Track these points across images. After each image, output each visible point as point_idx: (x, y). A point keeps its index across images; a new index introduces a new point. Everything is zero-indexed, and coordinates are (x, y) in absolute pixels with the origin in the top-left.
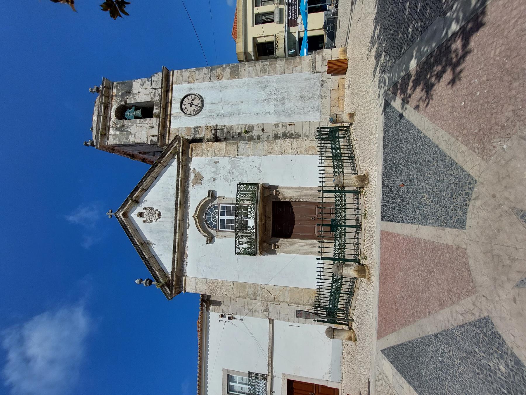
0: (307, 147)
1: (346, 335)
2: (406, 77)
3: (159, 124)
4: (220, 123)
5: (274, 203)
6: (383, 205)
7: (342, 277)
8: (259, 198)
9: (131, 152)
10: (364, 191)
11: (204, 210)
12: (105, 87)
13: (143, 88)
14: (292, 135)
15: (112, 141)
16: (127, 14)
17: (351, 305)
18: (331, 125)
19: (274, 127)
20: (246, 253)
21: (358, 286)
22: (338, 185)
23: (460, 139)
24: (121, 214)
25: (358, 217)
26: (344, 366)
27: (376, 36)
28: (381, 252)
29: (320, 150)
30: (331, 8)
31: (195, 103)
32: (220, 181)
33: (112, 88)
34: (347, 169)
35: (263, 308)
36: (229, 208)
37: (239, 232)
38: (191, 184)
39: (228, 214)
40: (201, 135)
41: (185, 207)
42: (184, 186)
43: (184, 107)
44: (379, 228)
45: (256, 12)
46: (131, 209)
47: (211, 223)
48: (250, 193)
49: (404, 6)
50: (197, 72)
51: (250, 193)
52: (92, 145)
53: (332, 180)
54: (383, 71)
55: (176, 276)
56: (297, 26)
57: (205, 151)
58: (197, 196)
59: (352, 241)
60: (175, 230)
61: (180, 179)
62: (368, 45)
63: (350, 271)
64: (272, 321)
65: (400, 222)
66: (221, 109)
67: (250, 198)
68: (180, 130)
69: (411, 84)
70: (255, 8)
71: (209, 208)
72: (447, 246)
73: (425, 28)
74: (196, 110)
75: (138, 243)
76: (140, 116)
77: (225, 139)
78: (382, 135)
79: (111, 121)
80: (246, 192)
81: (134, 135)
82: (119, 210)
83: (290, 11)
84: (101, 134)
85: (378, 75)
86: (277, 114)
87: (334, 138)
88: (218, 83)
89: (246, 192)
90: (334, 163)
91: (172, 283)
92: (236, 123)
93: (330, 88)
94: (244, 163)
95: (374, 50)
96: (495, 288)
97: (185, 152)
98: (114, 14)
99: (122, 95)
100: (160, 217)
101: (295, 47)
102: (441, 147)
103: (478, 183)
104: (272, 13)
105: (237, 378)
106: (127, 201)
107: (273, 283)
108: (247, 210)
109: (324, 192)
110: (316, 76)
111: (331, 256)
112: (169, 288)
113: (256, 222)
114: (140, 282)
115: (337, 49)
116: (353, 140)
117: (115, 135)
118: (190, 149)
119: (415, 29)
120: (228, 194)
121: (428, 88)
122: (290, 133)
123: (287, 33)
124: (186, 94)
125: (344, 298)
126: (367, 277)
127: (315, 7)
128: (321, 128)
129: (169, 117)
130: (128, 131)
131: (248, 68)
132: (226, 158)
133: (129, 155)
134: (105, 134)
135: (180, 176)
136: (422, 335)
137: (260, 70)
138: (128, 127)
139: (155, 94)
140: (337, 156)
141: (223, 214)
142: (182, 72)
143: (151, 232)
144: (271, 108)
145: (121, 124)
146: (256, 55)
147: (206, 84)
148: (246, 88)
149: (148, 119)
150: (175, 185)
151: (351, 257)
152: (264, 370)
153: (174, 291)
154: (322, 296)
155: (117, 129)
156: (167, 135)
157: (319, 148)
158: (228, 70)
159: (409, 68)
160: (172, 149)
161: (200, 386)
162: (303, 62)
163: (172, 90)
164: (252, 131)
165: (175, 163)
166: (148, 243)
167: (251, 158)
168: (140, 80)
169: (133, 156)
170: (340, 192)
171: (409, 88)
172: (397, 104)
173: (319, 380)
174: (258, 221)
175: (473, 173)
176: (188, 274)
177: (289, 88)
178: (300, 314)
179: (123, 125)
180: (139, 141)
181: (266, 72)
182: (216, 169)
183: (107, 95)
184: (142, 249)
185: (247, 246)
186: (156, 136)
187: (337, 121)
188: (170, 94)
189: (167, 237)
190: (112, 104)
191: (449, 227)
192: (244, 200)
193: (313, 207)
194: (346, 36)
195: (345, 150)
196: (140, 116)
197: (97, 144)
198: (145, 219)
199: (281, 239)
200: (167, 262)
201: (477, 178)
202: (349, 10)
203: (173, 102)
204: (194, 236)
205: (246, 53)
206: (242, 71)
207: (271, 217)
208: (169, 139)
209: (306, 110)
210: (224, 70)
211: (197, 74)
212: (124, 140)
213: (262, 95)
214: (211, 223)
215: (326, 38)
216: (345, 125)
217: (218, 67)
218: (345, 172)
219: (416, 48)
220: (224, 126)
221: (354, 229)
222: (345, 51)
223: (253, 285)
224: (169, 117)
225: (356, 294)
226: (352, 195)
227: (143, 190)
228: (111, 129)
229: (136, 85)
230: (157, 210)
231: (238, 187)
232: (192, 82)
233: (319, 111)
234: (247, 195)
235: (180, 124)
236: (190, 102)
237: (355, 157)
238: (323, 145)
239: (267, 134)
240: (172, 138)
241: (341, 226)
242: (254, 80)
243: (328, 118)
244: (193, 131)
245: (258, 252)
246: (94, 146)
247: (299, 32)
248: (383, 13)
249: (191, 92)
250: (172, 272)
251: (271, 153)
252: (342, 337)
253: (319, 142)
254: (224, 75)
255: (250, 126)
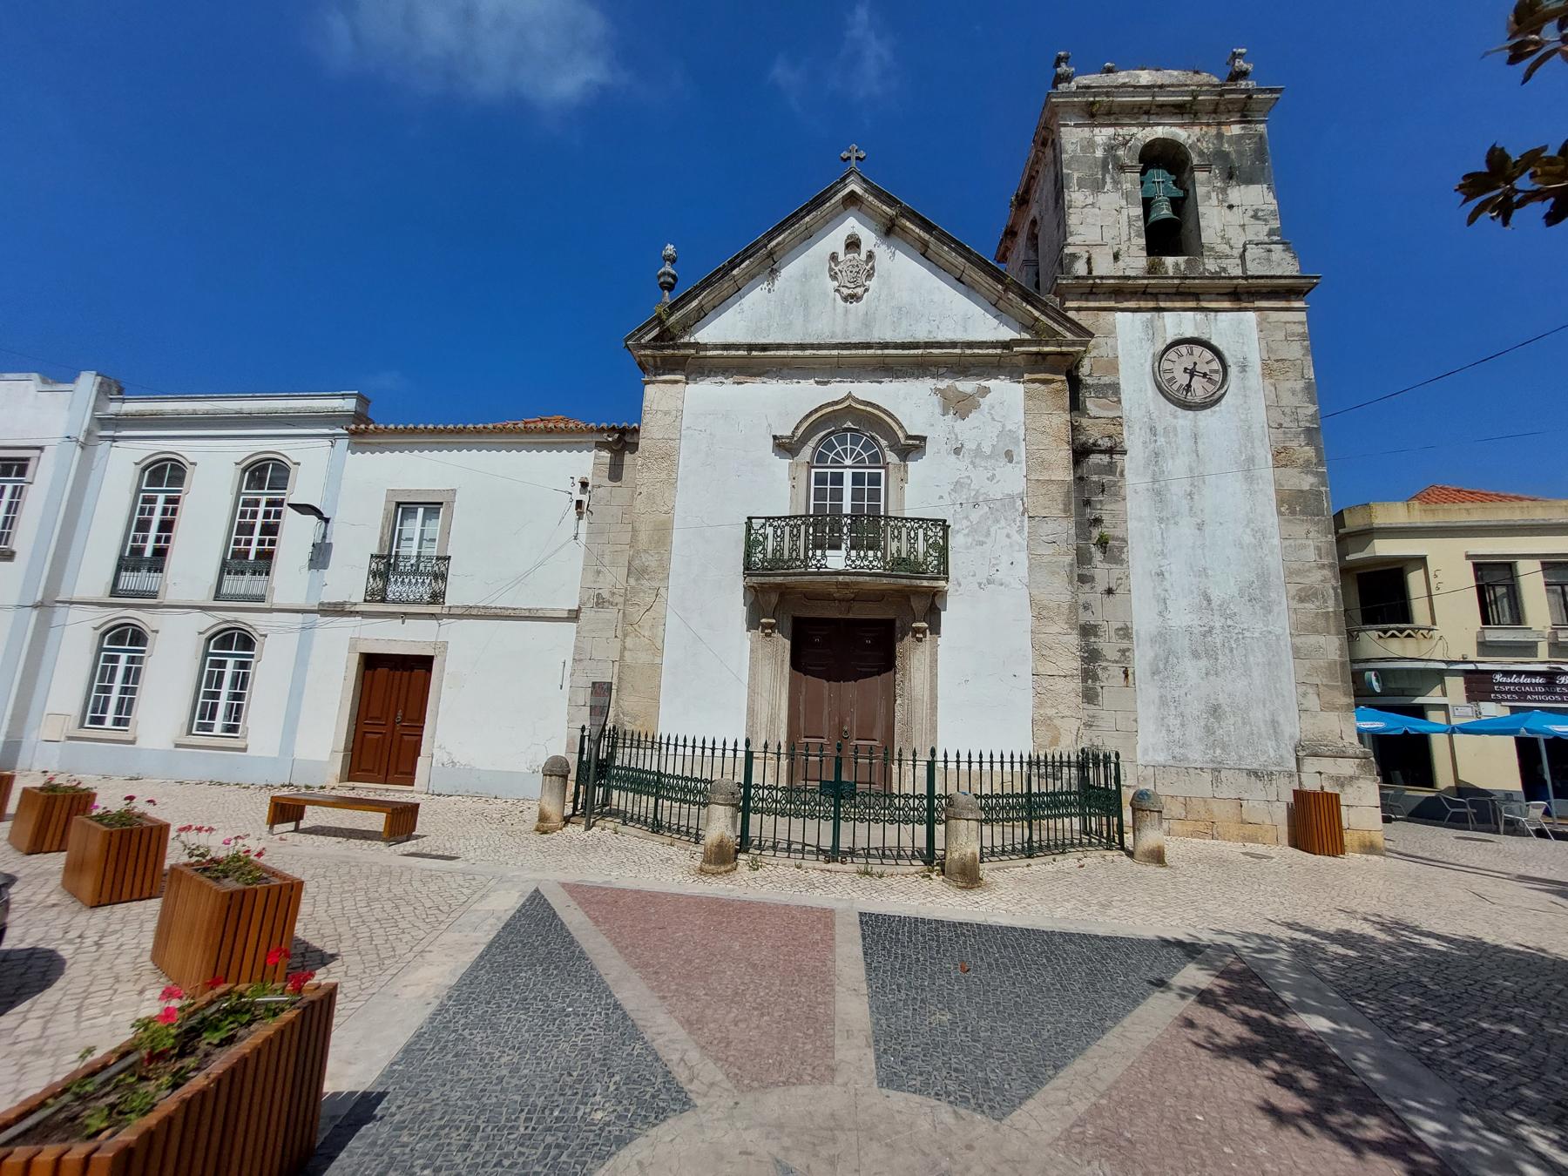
0: (1057, 722)
1: (552, 809)
2: (1279, 1004)
3: (1129, 278)
4: (1133, 465)
5: (891, 623)
6: (902, 921)
7: (706, 805)
8: (904, 581)
9: (1035, 196)
10: (933, 876)
11: (868, 425)
12: (1250, 97)
13: (1247, 220)
14: (1095, 678)
15: (1073, 137)
16: (1472, 218)
17: (625, 824)
18: (1127, 795)
19: (1120, 625)
20: (750, 546)
21: (677, 843)
22: (950, 805)
23: (1104, 1102)
24: (854, 186)
25: (859, 856)
26: (469, 801)
27: (1417, 939)
28: (777, 906)
29: (1049, 758)
30: (1535, 813)
31: (1197, 383)
32: (956, 467)
33: (1245, 120)
34: (995, 835)
35: (606, 595)
36: (875, 495)
37: (808, 526)
38: (944, 384)
39: (857, 495)
40: (1092, 406)
41: (874, 370)
42: (937, 365)
43: (1183, 349)
44: (839, 906)
45: (1523, 567)
46: (868, 216)
47: (831, 447)
48: (921, 558)
49: (1509, 1019)
50: (1300, 385)
51: (921, 558)
52: (1060, 79)
53: (964, 787)
54: (1299, 949)
55: (688, 356)
56: (1470, 699)
57: (1045, 420)
58: (909, 402)
59: (796, 837)
60: (812, 346)
61: (958, 351)
62: (1389, 914)
63: (719, 824)
64: (574, 616)
65: (865, 954)
66: (1176, 466)
67: (904, 555)
68: (1109, 341)
69: (1255, 1013)
70: (1536, 565)
71: (873, 438)
72: (830, 1049)
73: (1430, 1062)
74: (1175, 387)
75: (774, 243)
76: (1154, 217)
77: (1080, 480)
78: (1101, 932)
79: (1134, 130)
80: (921, 546)
81: (1093, 204)
82: (865, 181)
83: (1523, 679)
84: (1093, 103)
85: (1286, 934)
86: (1160, 634)
87: (1086, 800)
88: (1264, 455)
89: (921, 546)
90: (1013, 796)
91: (668, 347)
92: (1133, 512)
93: (1245, 796)
94: (1008, 536)
95: (1369, 930)
96: (761, 1125)
97: (1039, 362)
98: (1473, 185)
99: (1221, 156)
100: (845, 299)
101: (1389, 691)
102: (1079, 1061)
103: (996, 1123)
104: (1518, 617)
105: (435, 527)
106: (890, 201)
107: (672, 621)
108: (871, 549)
109: (931, 766)
110: (1287, 756)
111: (756, 779)
112: (654, 339)
113: (838, 573)
114: (667, 258)
115: (1380, 825)
116: (1080, 855)
117: (1091, 144)
118: (1050, 376)
119: (1429, 1038)
120: (916, 491)
121: (1249, 1053)
122: (1099, 672)
123: (1443, 666)
124: (1226, 354)
125: (636, 809)
126: (707, 867)
127: (1540, 761)
128: (1117, 765)
129: (1151, 304)
130: (1104, 183)
131: (1314, 544)
132: (1020, 486)
133: (1027, 191)
134: (1094, 112)
135: (968, 351)
136: (608, 980)
137: (1307, 581)
138: (1116, 182)
139: (1227, 257)
140: (1030, 807)
141: (857, 479)
142: (1302, 337)
143: (805, 277)
144: (1182, 617)
145: (1127, 162)
146: (1363, 567)
147: (1259, 415)
148: (1248, 539)
149: (1143, 241)
150: (940, 338)
151: (753, 831)
152: (455, 596)
153: (648, 352)
154: (649, 752)
155: (1110, 149)
156: (1092, 304)
157: (1057, 758)
158: (1307, 482)
159: (1305, 1012)
160: (1050, 322)
161: (414, 431)
162: (1333, 717)
163: (1239, 310)
164: (1105, 560)
165: (1007, 334)
166: (774, 272)
167: (1022, 558)
168: (1274, 206)
169: (1023, 201)
170: (931, 809)
171: (1245, 1009)
172: (1194, 976)
173: (433, 737)
174: (841, 578)
175: (1019, 1116)
176: (691, 387)
177: (1247, 672)
178: (601, 690)
179: (1122, 168)
180: (1073, 220)
181: (1301, 600)
182: (989, 457)
183: (1222, 107)
184: (759, 256)
185: (770, 549)
186: (1090, 271)
187: (1139, 814)
188: (1227, 305)
189: (791, 323)
190: (1193, 124)
191: (878, 1058)
192: (900, 540)
193: (877, 734)
194: (1426, 855)
195: (1044, 833)
196: (1154, 217)
197: (1063, 94)
198: (841, 257)
199: (788, 643)
200: (723, 328)
201: (1007, 1121)
202: (1522, 871)
203: (1200, 316)
204: (797, 399)
205: (1369, 533)
206: (1306, 526)
207: (851, 616)
208: (1078, 309)
209: (1174, 722)
210: (1306, 467)
211: (1293, 388)
212: (1076, 175)
213: (1224, 588)
214: (831, 447)
215: (1424, 793)
216: (1128, 839)
217: (1318, 450)
218: (987, 829)
219: (1366, 1035)
220: (1122, 474)
221: (827, 843)
222: (1370, 848)
223: (664, 567)
224: (1151, 304)
225: (657, 837)
226: (921, 842)
227: (926, 245)
228: (1111, 131)
229: (1257, 196)
230: (866, 290)
231: (935, 522)
232: (1268, 370)
233: (1171, 762)
234: (912, 549)
235: (1129, 341)
236: (1201, 368)
237: (1029, 857)
238: (1065, 770)
239: (1096, 605)
240: (1083, 319)
241: (837, 806)
242: (1274, 563)
243: (1150, 787)
244: (1106, 380)
245: (754, 579)
246: (1055, 86)
247: (1444, 707)
248: (1493, 965)
249: (1233, 371)
250: (696, 346)
251: (1038, 617)
252: (547, 798)
253: (1073, 758)
254: (1288, 471)
255: (1121, 552)
